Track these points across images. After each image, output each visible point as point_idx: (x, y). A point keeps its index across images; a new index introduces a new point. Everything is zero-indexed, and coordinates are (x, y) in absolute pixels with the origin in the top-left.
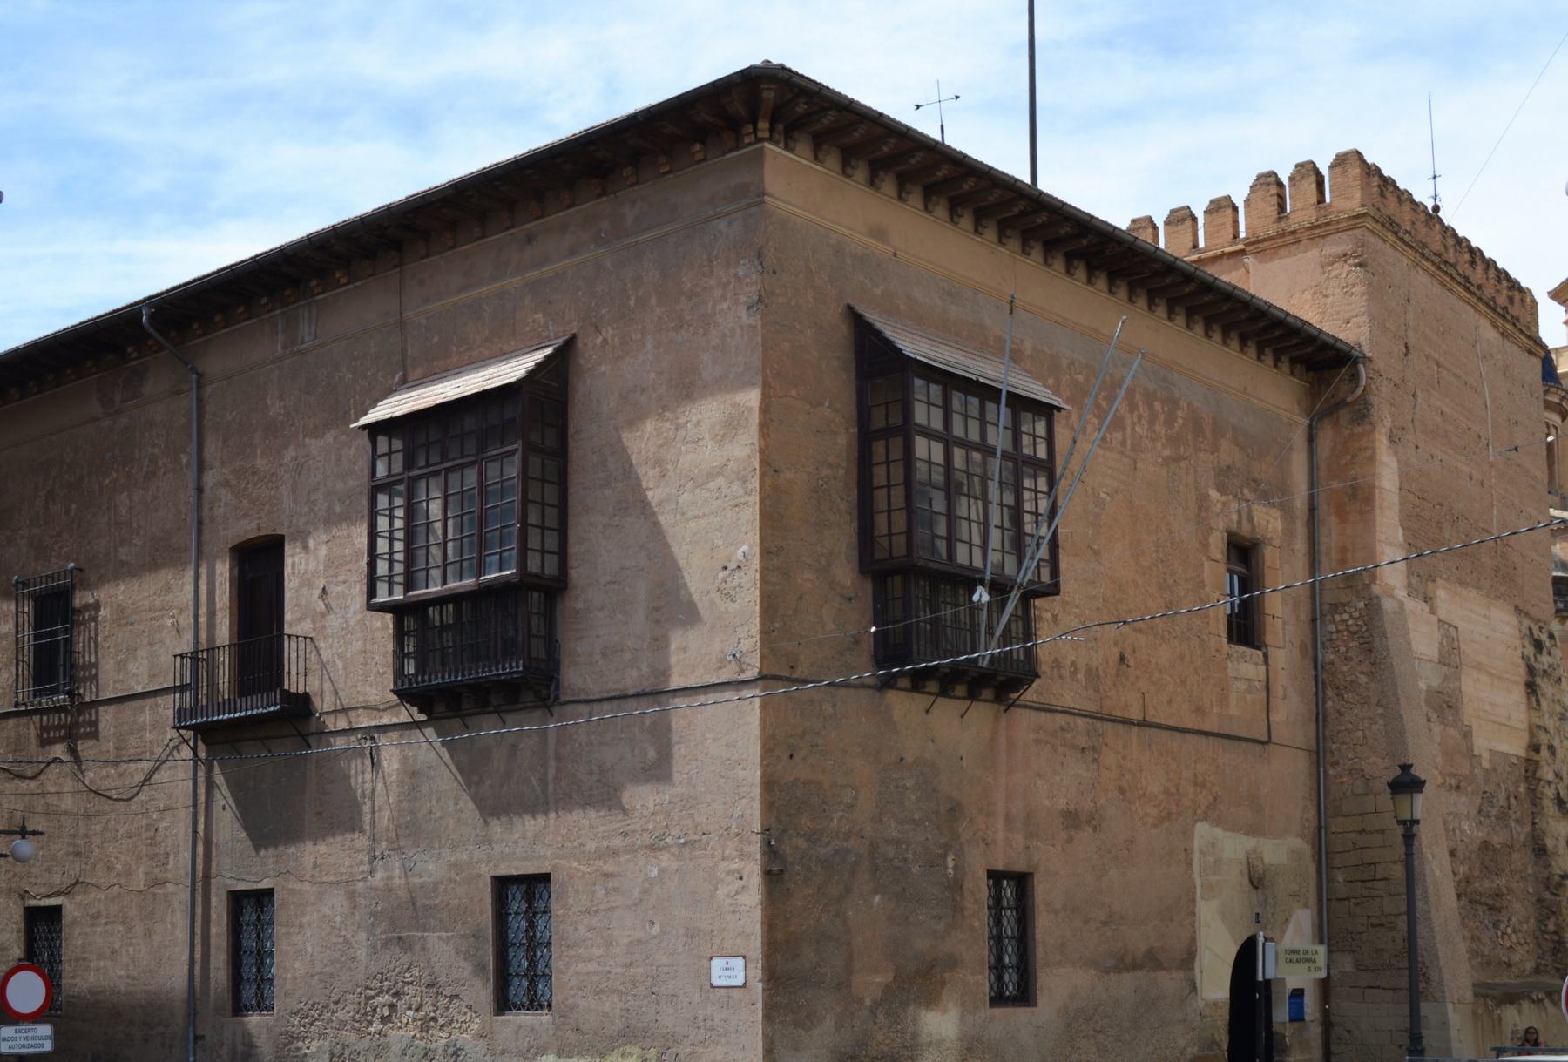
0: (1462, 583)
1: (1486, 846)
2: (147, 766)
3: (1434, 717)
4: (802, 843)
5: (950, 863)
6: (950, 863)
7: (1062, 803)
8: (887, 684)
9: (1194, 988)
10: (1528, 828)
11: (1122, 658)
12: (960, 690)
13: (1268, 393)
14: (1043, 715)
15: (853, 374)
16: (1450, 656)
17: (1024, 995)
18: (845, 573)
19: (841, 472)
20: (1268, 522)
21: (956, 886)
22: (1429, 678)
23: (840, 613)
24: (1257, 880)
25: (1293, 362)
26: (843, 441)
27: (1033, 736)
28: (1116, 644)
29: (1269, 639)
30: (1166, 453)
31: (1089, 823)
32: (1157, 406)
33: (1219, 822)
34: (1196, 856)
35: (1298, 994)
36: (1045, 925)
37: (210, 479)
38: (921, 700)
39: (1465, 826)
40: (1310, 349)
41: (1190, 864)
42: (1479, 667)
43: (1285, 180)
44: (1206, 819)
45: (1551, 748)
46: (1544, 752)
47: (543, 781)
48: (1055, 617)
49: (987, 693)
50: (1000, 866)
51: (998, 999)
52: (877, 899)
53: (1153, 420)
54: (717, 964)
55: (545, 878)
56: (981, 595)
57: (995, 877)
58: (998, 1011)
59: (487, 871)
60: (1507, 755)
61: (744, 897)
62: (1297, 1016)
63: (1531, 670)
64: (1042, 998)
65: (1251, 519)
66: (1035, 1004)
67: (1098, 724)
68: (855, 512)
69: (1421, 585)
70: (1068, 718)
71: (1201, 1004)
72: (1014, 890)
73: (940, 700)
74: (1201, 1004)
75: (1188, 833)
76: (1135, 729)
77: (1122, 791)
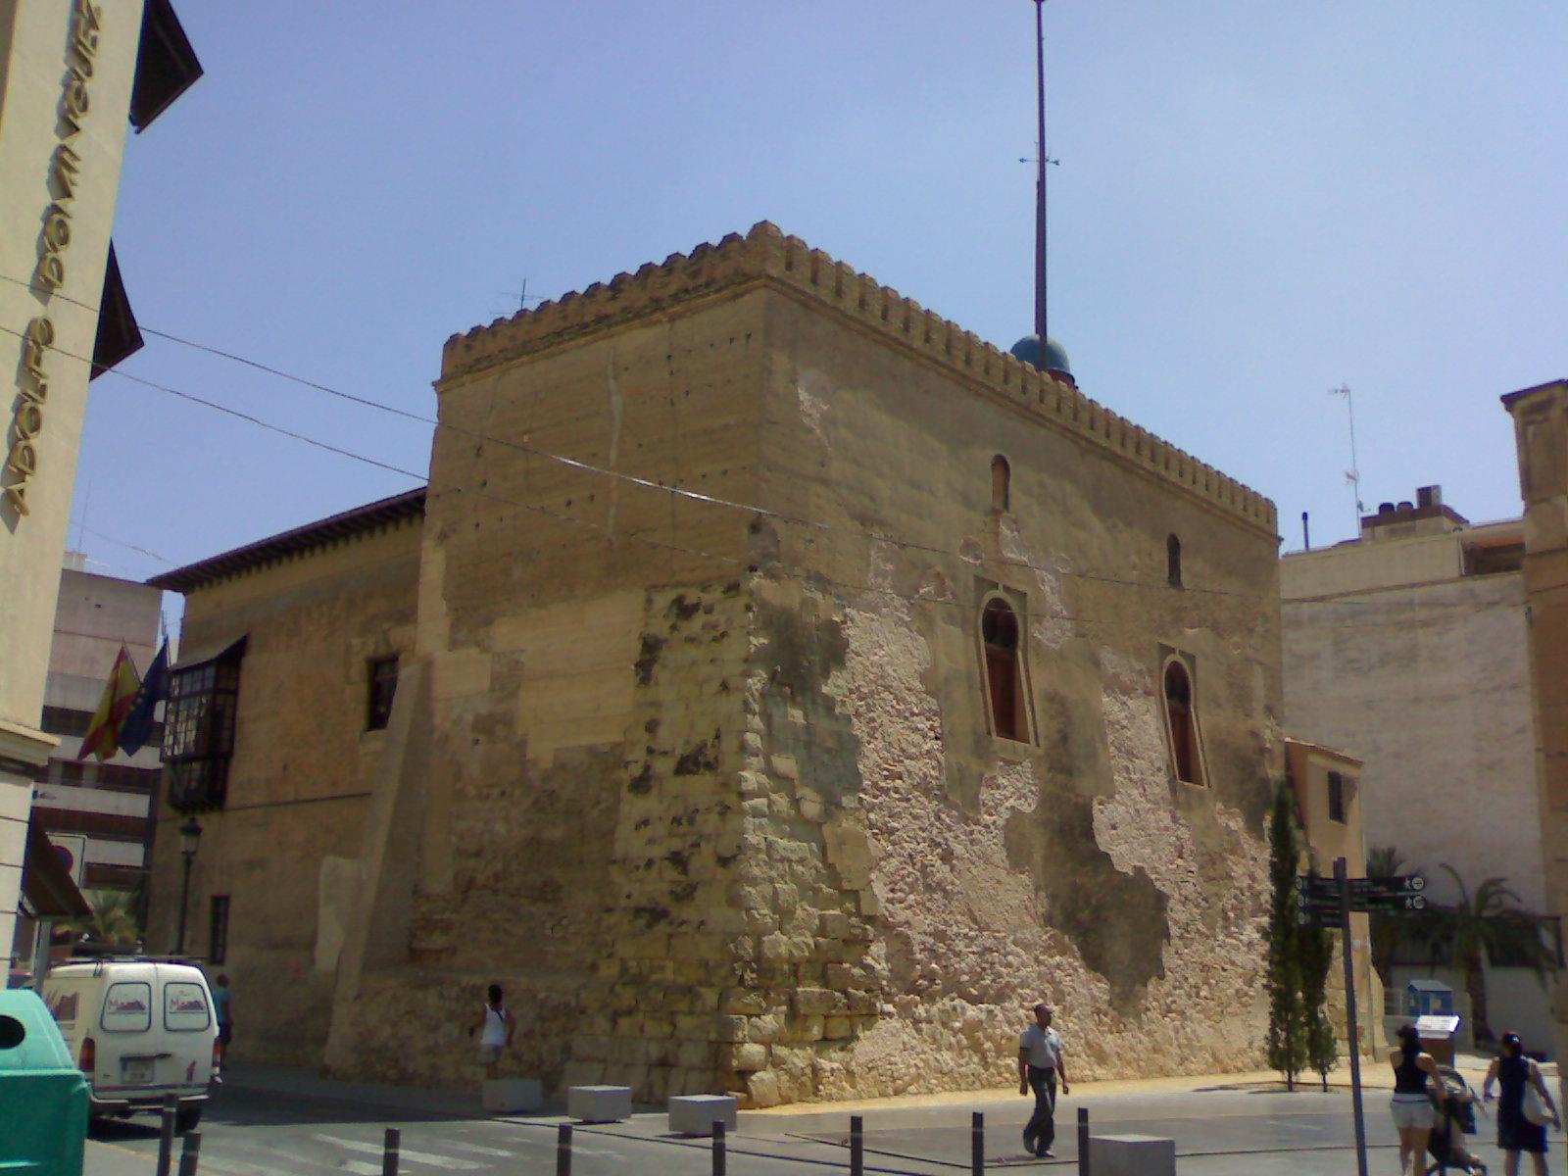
11: (285, 767)
72: (220, 903)
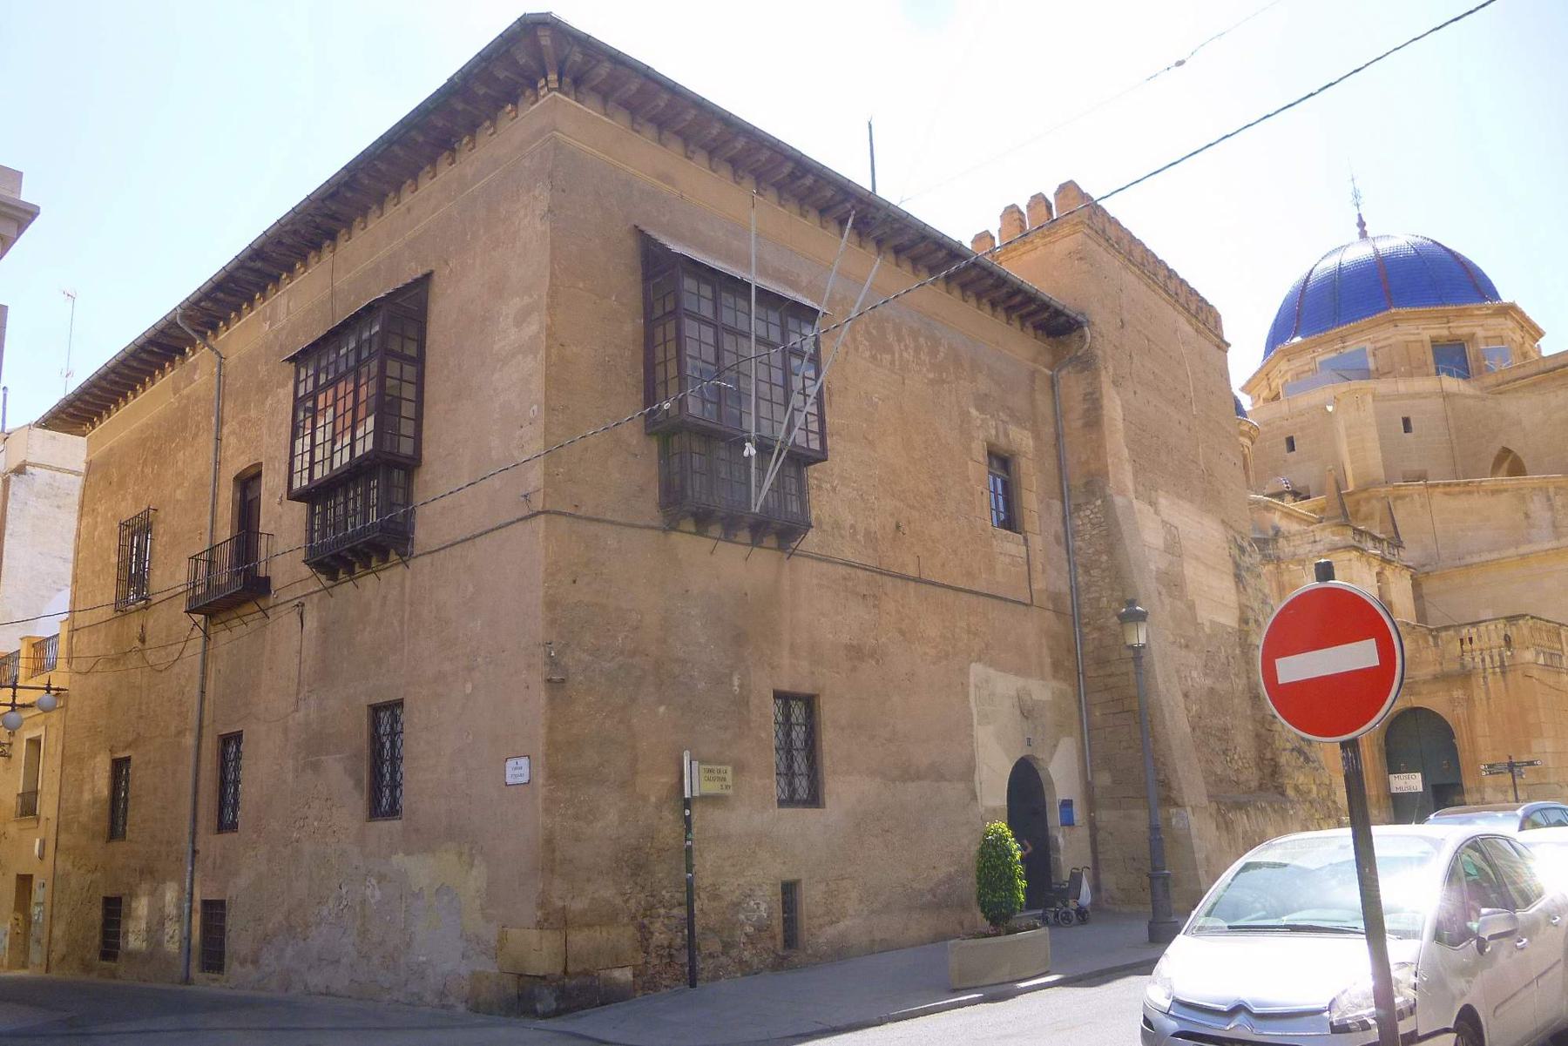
0: (1179, 496)
1: (1212, 690)
2: (180, 646)
3: (1164, 592)
4: (586, 657)
5: (736, 682)
6: (736, 682)
7: (845, 638)
8: (671, 526)
9: (974, 797)
10: (1244, 680)
11: (898, 527)
12: (744, 536)
13: (1016, 347)
14: (825, 565)
15: (639, 278)
16: (1173, 547)
17: (814, 799)
18: (632, 434)
19: (627, 353)
20: (1022, 440)
21: (742, 701)
22: (1156, 562)
23: (627, 471)
24: (1027, 712)
25: (1036, 327)
26: (631, 327)
27: (815, 581)
28: (892, 515)
29: (1027, 527)
30: (931, 376)
31: (872, 656)
32: (922, 340)
33: (992, 664)
34: (972, 690)
35: (1067, 804)
36: (829, 739)
37: (225, 431)
38: (705, 544)
39: (1194, 674)
40: (1046, 315)
41: (967, 696)
42: (1197, 558)
43: (1024, 210)
44: (979, 660)
45: (1256, 621)
46: (1252, 624)
47: (402, 623)
48: (834, 489)
49: (771, 541)
50: (785, 687)
51: (789, 801)
52: (662, 709)
53: (917, 350)
54: (511, 764)
55: (399, 704)
56: (750, 450)
57: (784, 697)
58: (787, 811)
59: (364, 701)
60: (1223, 626)
61: (531, 704)
62: (1068, 822)
63: (1237, 565)
64: (829, 800)
65: (1007, 435)
66: (824, 806)
67: (878, 577)
68: (642, 385)
69: (1147, 492)
70: (849, 570)
71: (982, 810)
72: (800, 712)
73: (720, 544)
74: (982, 810)
75: (964, 672)
76: (912, 584)
77: (902, 633)
